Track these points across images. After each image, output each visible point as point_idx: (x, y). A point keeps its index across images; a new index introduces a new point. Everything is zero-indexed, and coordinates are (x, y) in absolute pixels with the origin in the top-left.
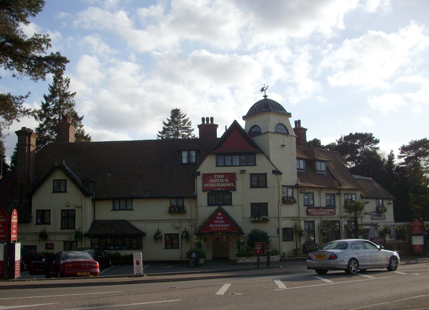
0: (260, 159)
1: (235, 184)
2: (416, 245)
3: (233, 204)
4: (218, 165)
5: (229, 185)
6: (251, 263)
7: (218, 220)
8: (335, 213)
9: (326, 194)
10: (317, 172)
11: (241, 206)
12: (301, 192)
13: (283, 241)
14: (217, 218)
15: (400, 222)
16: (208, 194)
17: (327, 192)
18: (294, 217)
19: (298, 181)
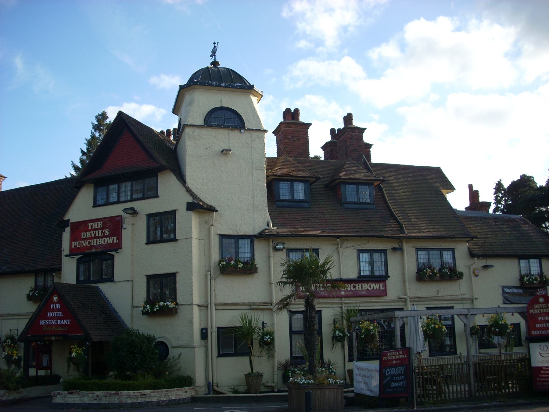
0: (167, 183)
1: (120, 238)
2: (541, 368)
3: (116, 278)
4: (98, 204)
5: (109, 240)
6: (77, 404)
7: (53, 310)
8: (384, 293)
10: (345, 206)
11: (130, 283)
12: (276, 249)
13: (219, 355)
14: (52, 306)
16: (79, 262)
18: (254, 304)
19: (268, 225)
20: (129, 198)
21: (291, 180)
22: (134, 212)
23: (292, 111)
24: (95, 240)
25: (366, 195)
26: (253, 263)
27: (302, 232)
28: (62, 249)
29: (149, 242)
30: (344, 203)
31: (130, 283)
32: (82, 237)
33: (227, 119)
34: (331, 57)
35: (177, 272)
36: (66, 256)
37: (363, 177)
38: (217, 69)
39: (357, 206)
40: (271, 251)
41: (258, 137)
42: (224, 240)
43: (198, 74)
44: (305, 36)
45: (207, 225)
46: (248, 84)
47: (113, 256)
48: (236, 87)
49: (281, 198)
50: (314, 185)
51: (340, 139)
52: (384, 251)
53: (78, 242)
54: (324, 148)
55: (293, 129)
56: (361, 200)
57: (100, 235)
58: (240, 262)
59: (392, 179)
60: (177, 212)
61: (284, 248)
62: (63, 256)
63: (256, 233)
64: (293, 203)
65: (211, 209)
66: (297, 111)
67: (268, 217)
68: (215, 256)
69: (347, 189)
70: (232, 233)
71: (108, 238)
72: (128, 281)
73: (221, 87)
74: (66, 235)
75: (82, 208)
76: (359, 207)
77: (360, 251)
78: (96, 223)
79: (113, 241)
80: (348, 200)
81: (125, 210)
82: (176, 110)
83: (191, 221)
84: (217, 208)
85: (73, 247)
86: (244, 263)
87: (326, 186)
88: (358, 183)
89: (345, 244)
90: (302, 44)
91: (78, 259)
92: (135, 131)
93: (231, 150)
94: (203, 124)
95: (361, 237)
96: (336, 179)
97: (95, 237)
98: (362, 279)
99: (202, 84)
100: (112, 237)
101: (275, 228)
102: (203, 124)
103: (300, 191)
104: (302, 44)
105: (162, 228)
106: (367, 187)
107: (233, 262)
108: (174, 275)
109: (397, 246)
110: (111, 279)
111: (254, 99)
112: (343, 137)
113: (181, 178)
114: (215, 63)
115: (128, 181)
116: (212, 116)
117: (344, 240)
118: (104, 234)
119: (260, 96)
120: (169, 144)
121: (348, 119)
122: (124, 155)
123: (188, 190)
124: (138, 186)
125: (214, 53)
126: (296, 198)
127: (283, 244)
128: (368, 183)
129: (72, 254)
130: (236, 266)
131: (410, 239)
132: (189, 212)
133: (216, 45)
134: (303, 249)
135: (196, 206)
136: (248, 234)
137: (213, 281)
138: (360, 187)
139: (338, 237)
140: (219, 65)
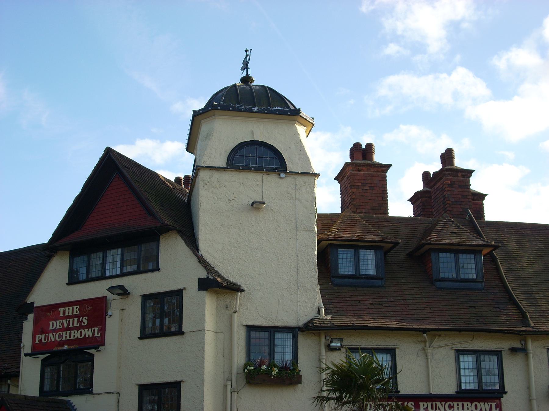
1: (103, 330)
3: (95, 389)
5: (88, 333)
9: (429, 347)
10: (438, 284)
11: (115, 396)
12: (330, 349)
15: (64, 400)
17: (460, 347)
19: (319, 312)
20: (118, 272)
21: (356, 246)
22: (123, 292)
23: (364, 147)
24: (68, 332)
25: (470, 268)
26: (294, 369)
27: (371, 322)
28: (22, 345)
29: (144, 336)
30: (436, 280)
31: (115, 396)
32: (51, 328)
33: (262, 159)
34: (436, 68)
35: (182, 381)
36: (26, 355)
37: (464, 241)
38: (248, 88)
39: (457, 285)
40: (323, 350)
41: (305, 184)
42: (253, 334)
43: (221, 94)
44: (396, 38)
45: (227, 312)
46: (292, 108)
47: (93, 355)
48: (274, 113)
49: (341, 272)
50: (389, 254)
51: (436, 187)
52: (498, 353)
53: (44, 335)
54: (413, 200)
55: (364, 173)
56: (462, 276)
57: (75, 325)
58: (275, 366)
59: (513, 245)
60: (184, 292)
61: (342, 347)
62: (22, 355)
63: (301, 323)
64: (358, 280)
65: (234, 289)
66: (370, 146)
67: (319, 300)
68: (239, 358)
69: (441, 260)
70: (265, 324)
71: (86, 330)
72: (112, 393)
73: (252, 112)
74: (28, 326)
75: (52, 287)
76: (461, 286)
77: (459, 352)
78: (71, 308)
79: (93, 334)
80: (442, 276)
81: (111, 289)
82: (190, 147)
83: (204, 304)
84: (244, 287)
85: (37, 342)
86: (281, 369)
87: (410, 255)
88: (457, 250)
89: (437, 342)
90: (392, 49)
91: (43, 361)
92: (129, 177)
93: (264, 203)
94: (225, 166)
95: (460, 330)
96: (424, 245)
97: (68, 329)
98: (462, 396)
99: (224, 108)
100: (91, 328)
101: (329, 317)
102: (225, 166)
103: (369, 263)
104: (392, 49)
105: (164, 316)
106: (472, 256)
107: (264, 367)
108: (177, 385)
109: (518, 345)
110: (87, 390)
111: (301, 130)
112: (439, 184)
113: (192, 242)
114: (247, 80)
115: (117, 247)
116: (239, 154)
117: (435, 336)
118: (81, 325)
119: (309, 125)
120: (181, 196)
121: (447, 157)
122: (122, 212)
123: (202, 261)
124: (131, 255)
125: (246, 65)
126: (362, 272)
127: (341, 340)
128: (474, 250)
129: (35, 352)
130: (268, 373)
131: (538, 334)
132: (202, 292)
133: (248, 53)
134: (357, 349)
135: (214, 284)
136: (288, 325)
137: (235, 395)
138: (461, 256)
139: (424, 331)
140: (252, 81)
